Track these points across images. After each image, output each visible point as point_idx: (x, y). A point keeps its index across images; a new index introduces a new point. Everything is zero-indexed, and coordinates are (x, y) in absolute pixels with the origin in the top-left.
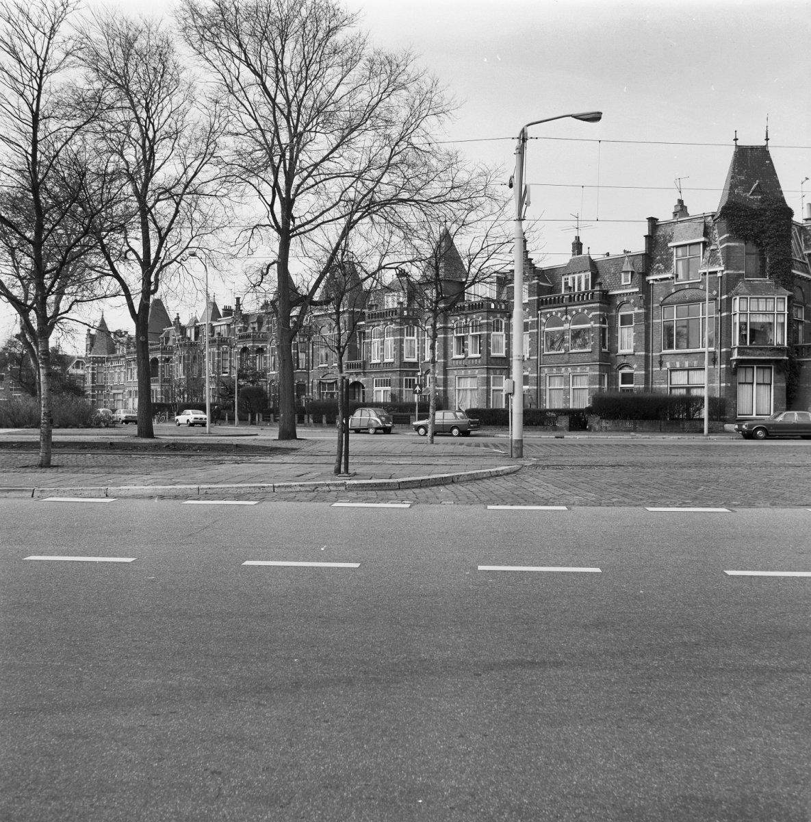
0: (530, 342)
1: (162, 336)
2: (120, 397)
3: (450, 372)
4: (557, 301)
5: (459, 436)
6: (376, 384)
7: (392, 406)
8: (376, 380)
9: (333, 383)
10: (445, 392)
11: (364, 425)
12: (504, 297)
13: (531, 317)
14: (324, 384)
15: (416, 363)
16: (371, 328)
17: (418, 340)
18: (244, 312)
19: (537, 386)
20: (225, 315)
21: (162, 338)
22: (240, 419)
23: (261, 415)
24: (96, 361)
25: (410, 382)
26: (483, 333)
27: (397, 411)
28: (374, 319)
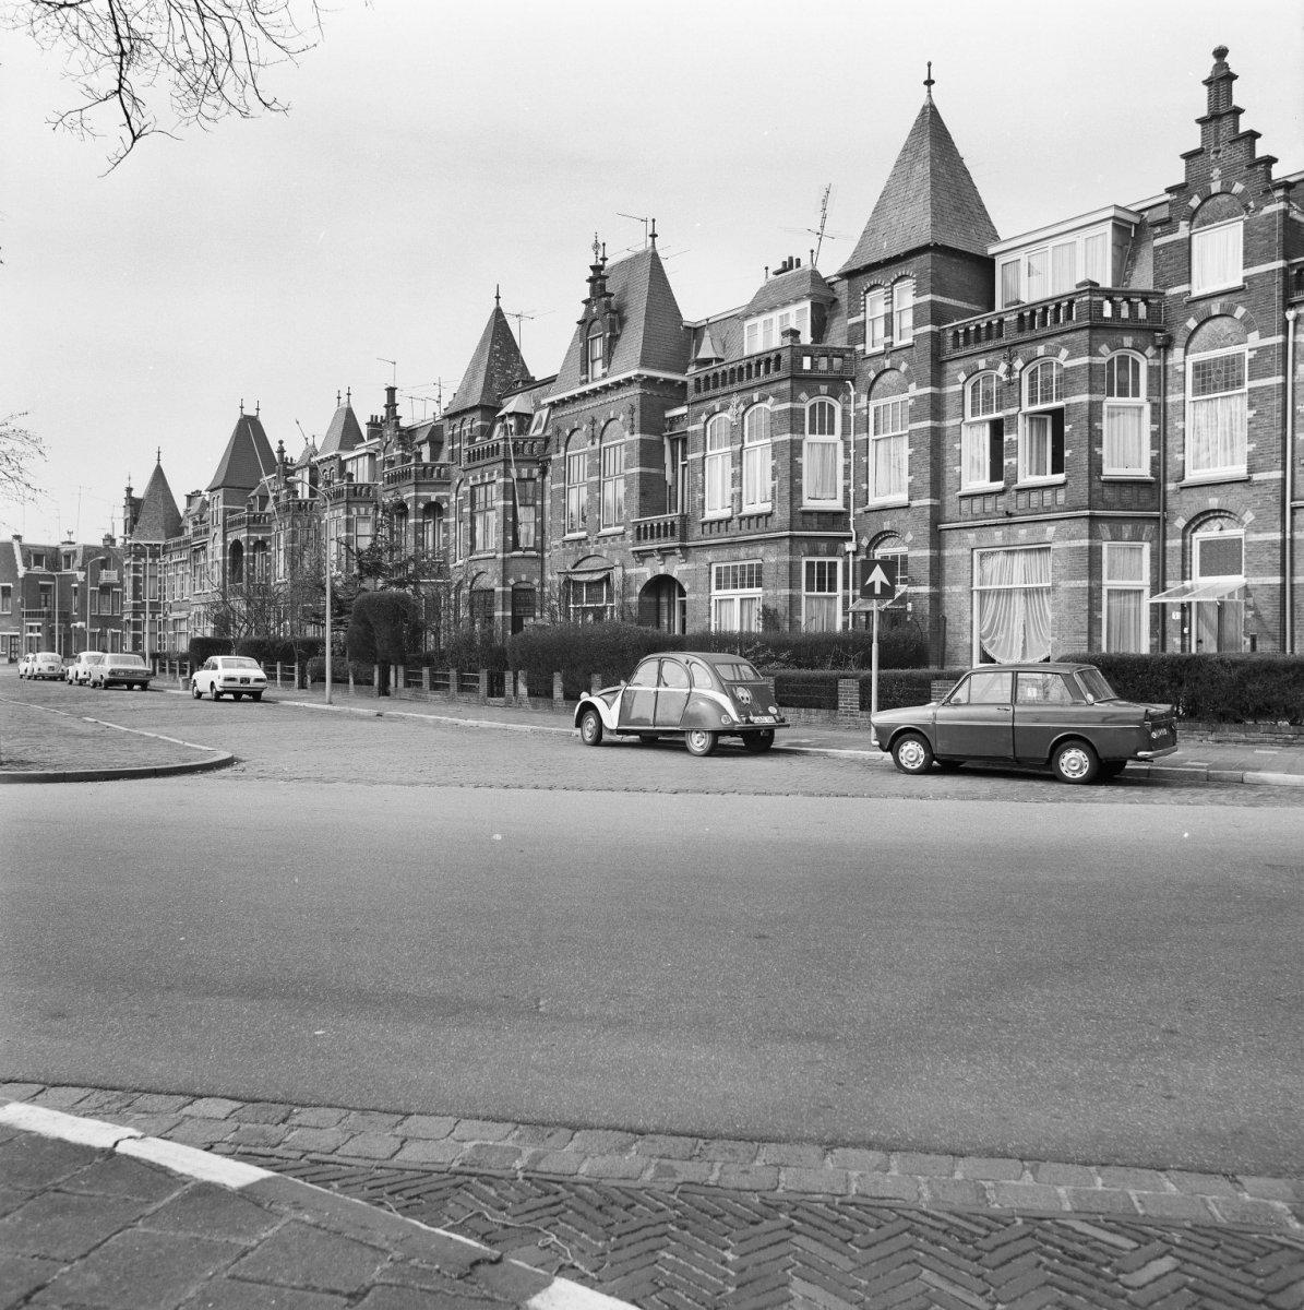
0: (910, 457)
1: (253, 493)
2: (184, 626)
3: (952, 538)
6: (718, 581)
7: (767, 644)
8: (718, 569)
9: (599, 583)
10: (937, 599)
11: (670, 716)
12: (1143, 279)
13: (913, 386)
14: (578, 584)
15: (839, 513)
16: (704, 417)
17: (847, 444)
18: (404, 423)
19: (1283, 574)
20: (372, 435)
21: (254, 497)
22: (335, 680)
23: (401, 670)
24: (137, 551)
25: (821, 573)
26: (1073, 400)
27: (787, 662)
28: (711, 393)
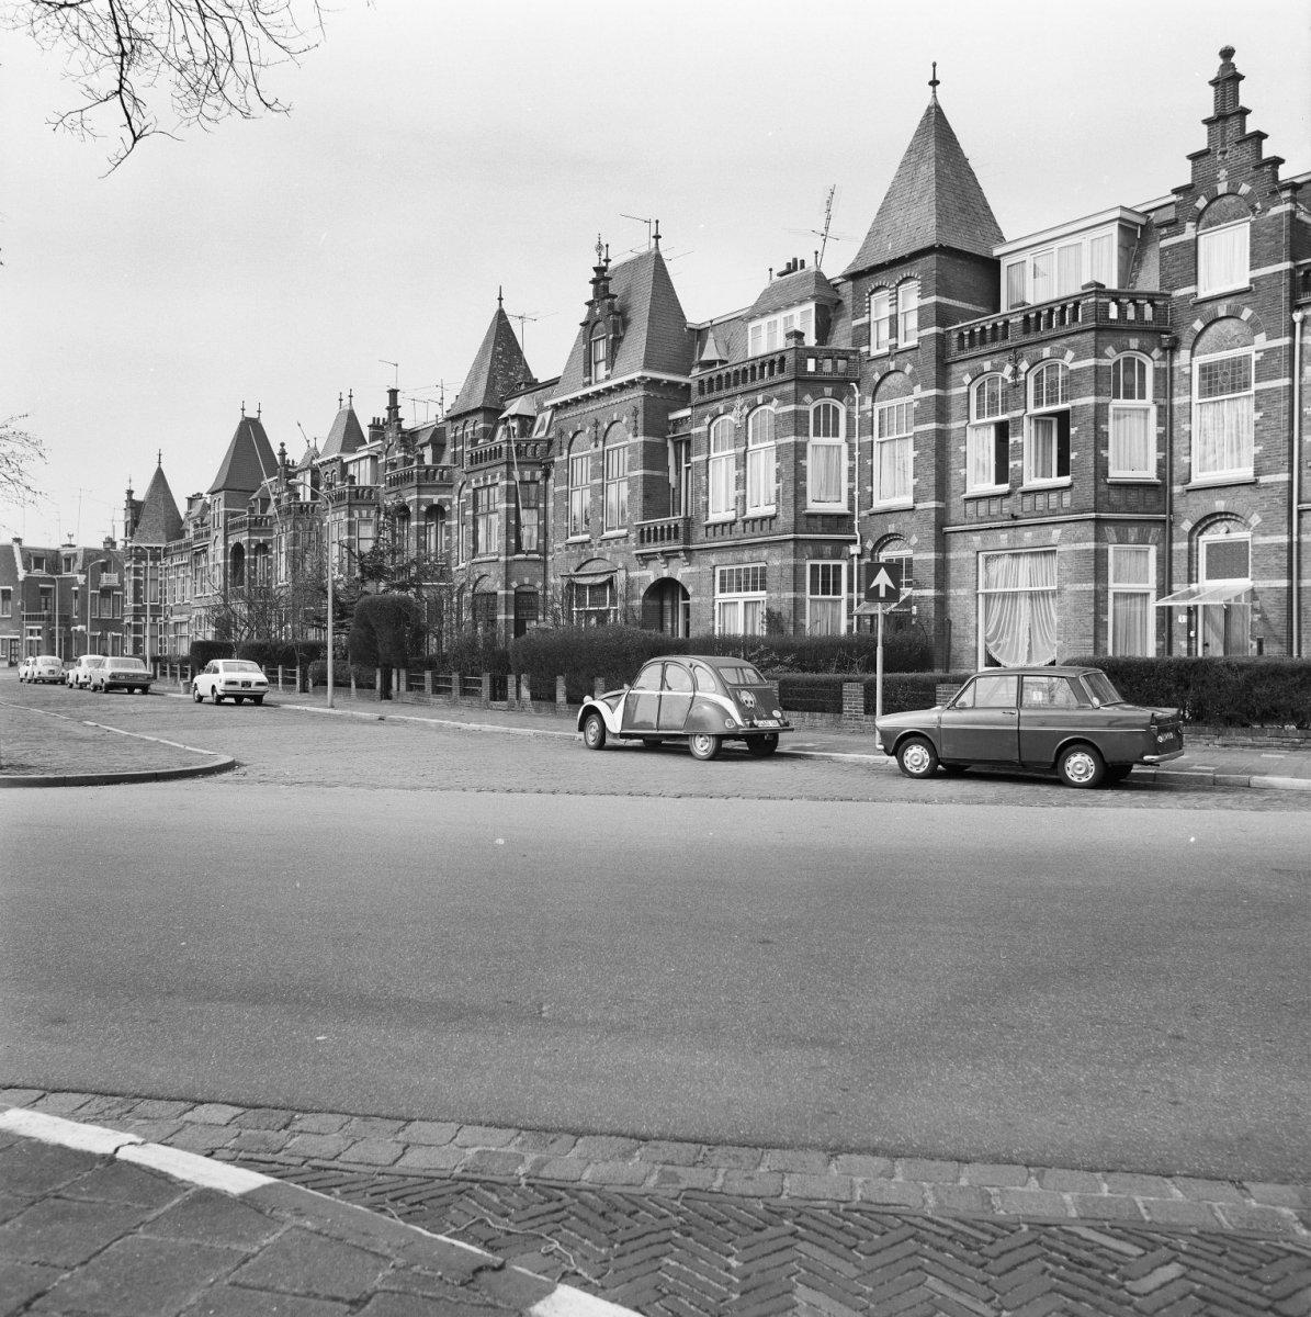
0: (915, 459)
1: (255, 496)
2: (185, 630)
3: (957, 541)
4: (1032, 324)
5: (932, 774)
6: (722, 584)
7: (771, 648)
8: (722, 572)
9: (602, 586)
10: (942, 603)
11: (674, 720)
12: (1149, 280)
13: (918, 388)
14: (581, 587)
15: (844, 516)
16: (708, 419)
17: (851, 446)
18: (406, 425)
19: (1290, 577)
20: (374, 438)
21: (256, 500)
22: (336, 684)
23: (403, 673)
24: (138, 554)
25: (826, 576)
26: (1079, 402)
27: (791, 666)
28: (715, 395)
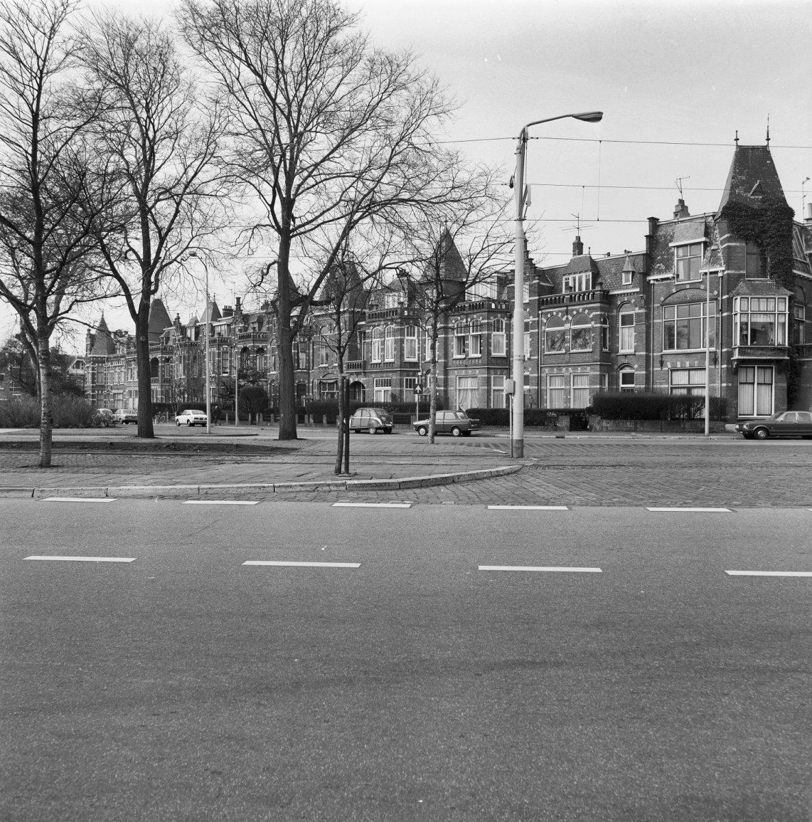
0: (530, 342)
1: (162, 336)
2: (120, 397)
3: (450, 372)
5: (459, 436)
6: (376, 384)
7: (393, 406)
8: (376, 380)
9: (333, 383)
10: (446, 392)
11: (365, 425)
12: (505, 297)
13: (531, 317)
14: (324, 384)
15: (416, 363)
16: (372, 328)
17: (419, 340)
18: (244, 312)
19: (538, 386)
20: (225, 315)
21: (163, 338)
22: (240, 419)
23: (261, 415)
24: (96, 361)
25: (410, 382)
26: (484, 333)
27: (397, 411)
28: (374, 319)
